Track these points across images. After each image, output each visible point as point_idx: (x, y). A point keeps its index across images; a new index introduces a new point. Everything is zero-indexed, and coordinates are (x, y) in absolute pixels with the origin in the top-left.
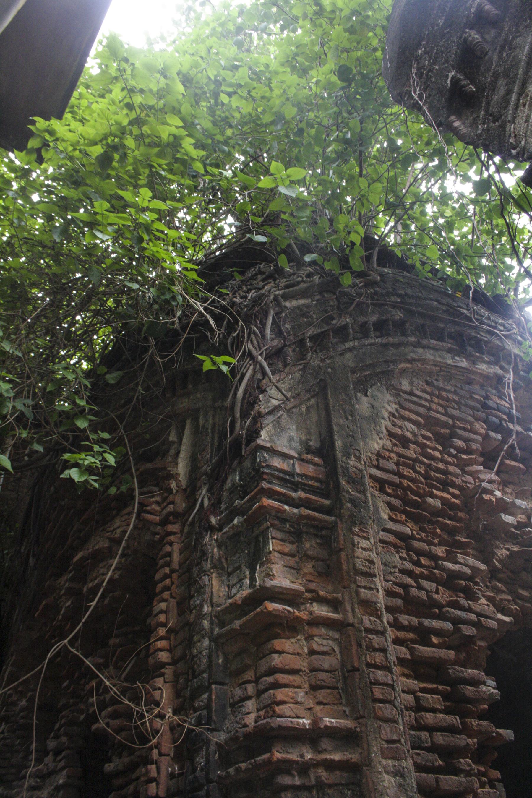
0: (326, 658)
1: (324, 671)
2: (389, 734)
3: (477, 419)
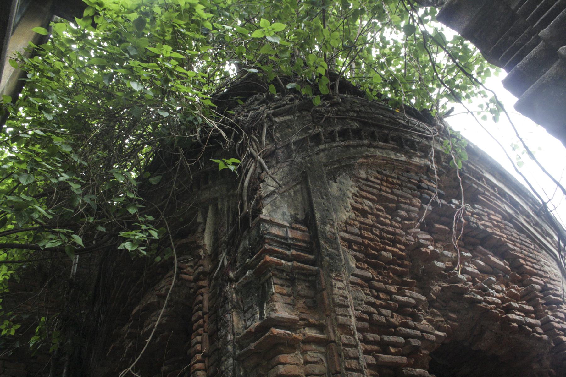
3: (414, 196)
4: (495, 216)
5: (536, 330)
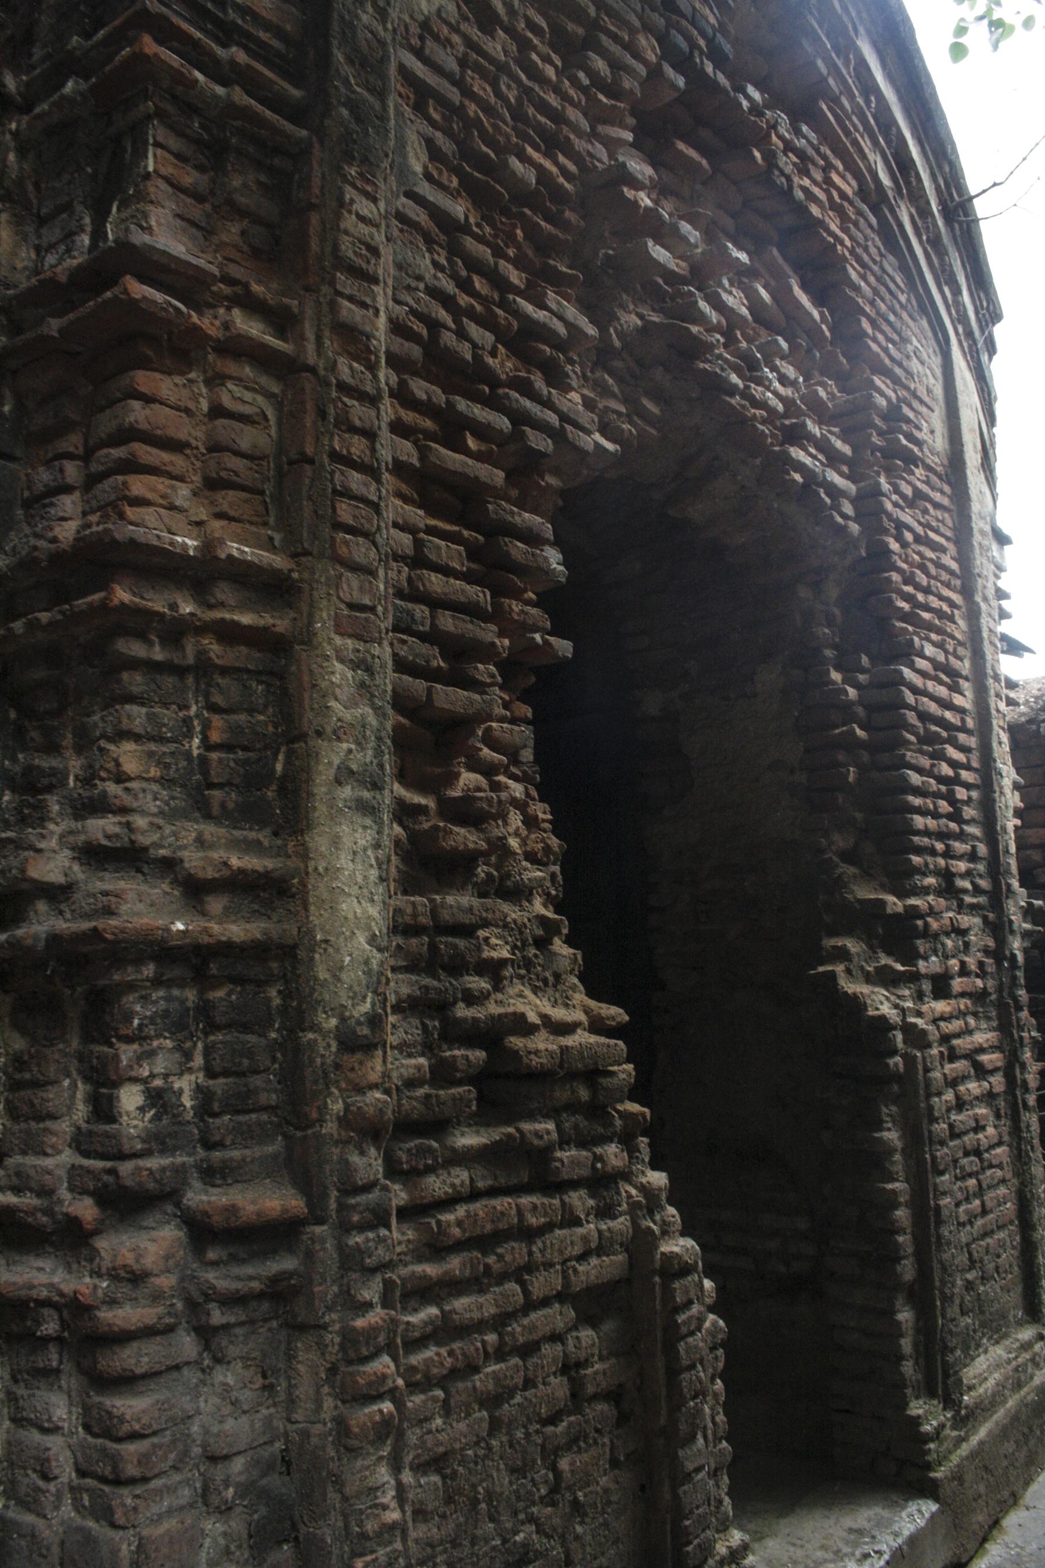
0: (248, 429)
1: (238, 453)
2: (355, 593)
3: (648, 28)
4: (843, 177)
5: (839, 505)
